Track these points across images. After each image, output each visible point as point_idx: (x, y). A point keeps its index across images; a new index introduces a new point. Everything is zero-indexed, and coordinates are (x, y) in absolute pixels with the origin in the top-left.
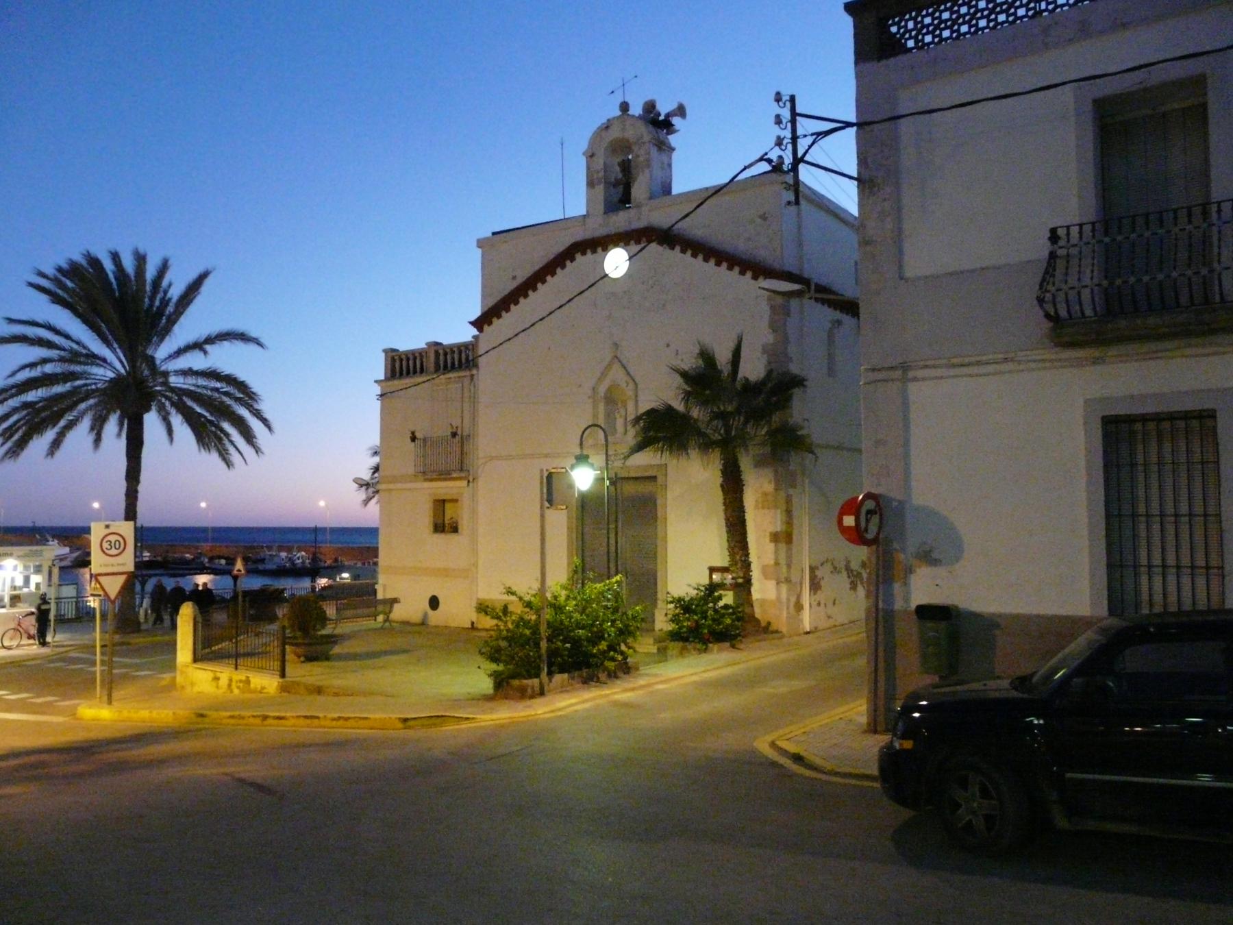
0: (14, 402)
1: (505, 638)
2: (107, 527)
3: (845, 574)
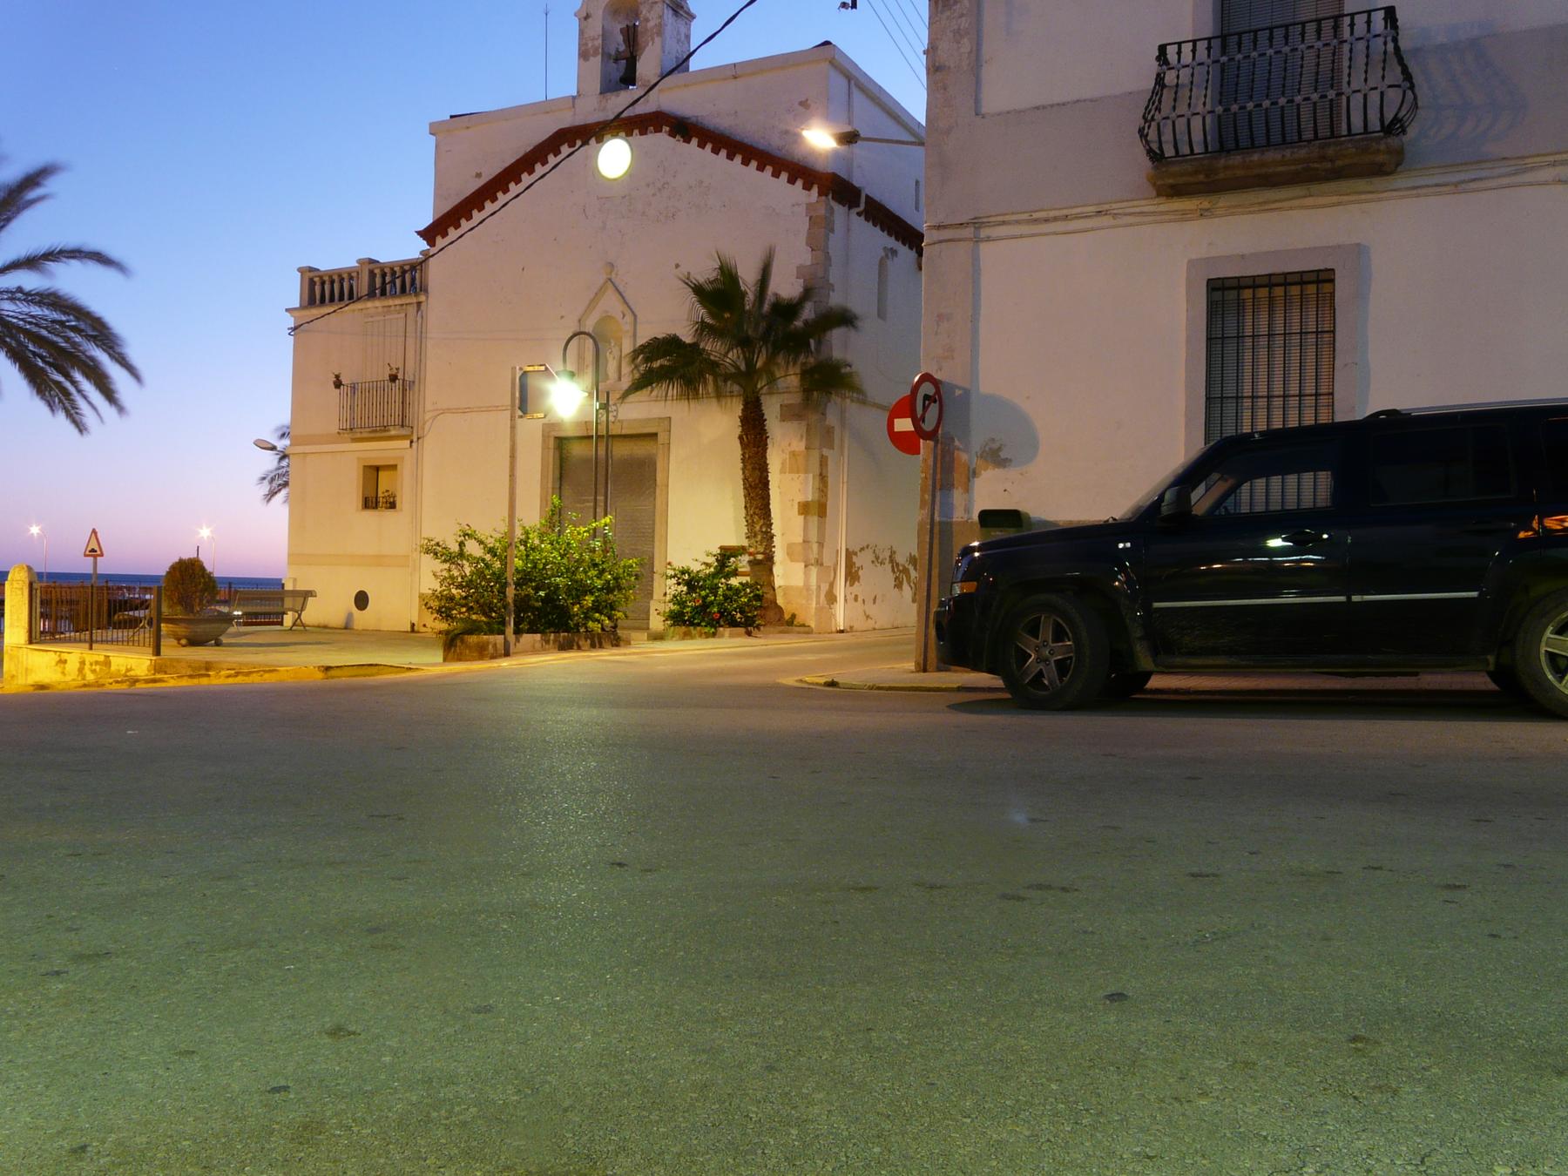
1: (460, 586)
3: (888, 567)
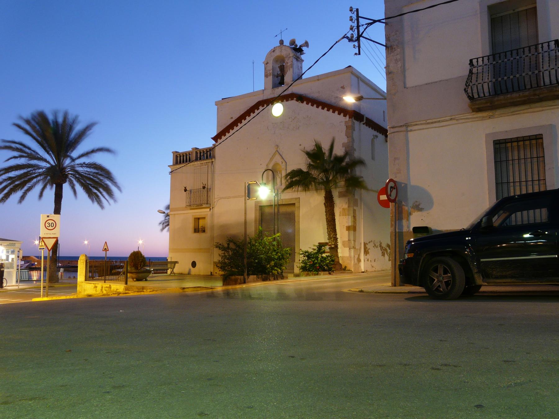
0: (5, 177)
2: (48, 216)
3: (379, 248)
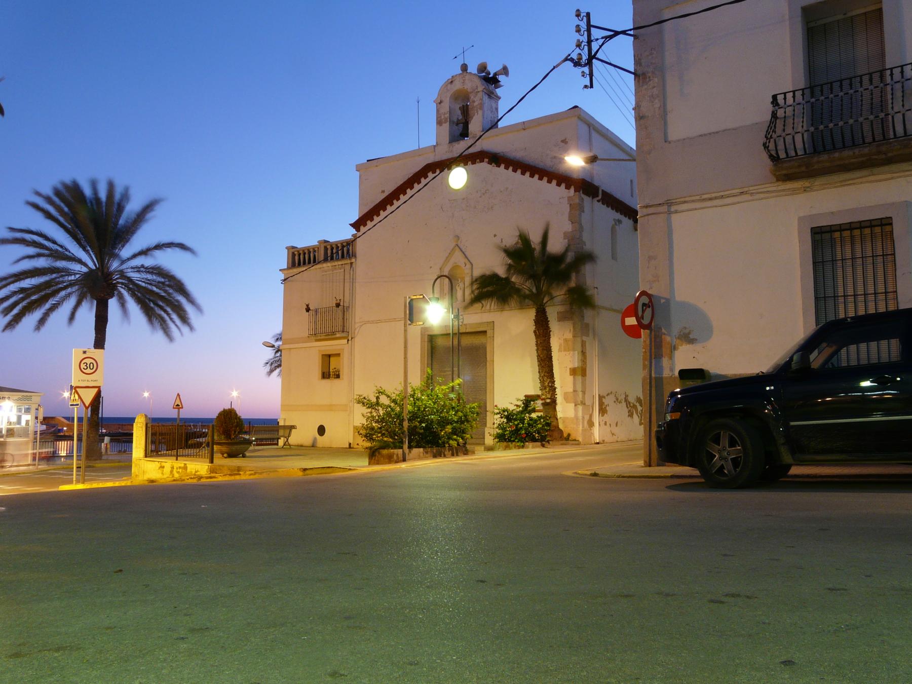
0: (13, 287)
1: (377, 422)
2: (85, 352)
3: (624, 404)
